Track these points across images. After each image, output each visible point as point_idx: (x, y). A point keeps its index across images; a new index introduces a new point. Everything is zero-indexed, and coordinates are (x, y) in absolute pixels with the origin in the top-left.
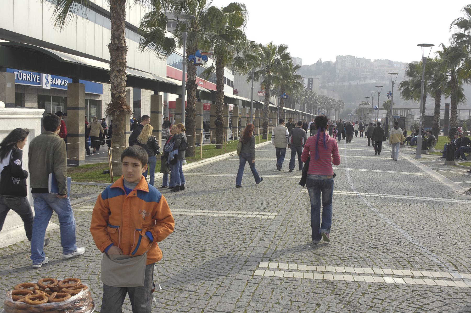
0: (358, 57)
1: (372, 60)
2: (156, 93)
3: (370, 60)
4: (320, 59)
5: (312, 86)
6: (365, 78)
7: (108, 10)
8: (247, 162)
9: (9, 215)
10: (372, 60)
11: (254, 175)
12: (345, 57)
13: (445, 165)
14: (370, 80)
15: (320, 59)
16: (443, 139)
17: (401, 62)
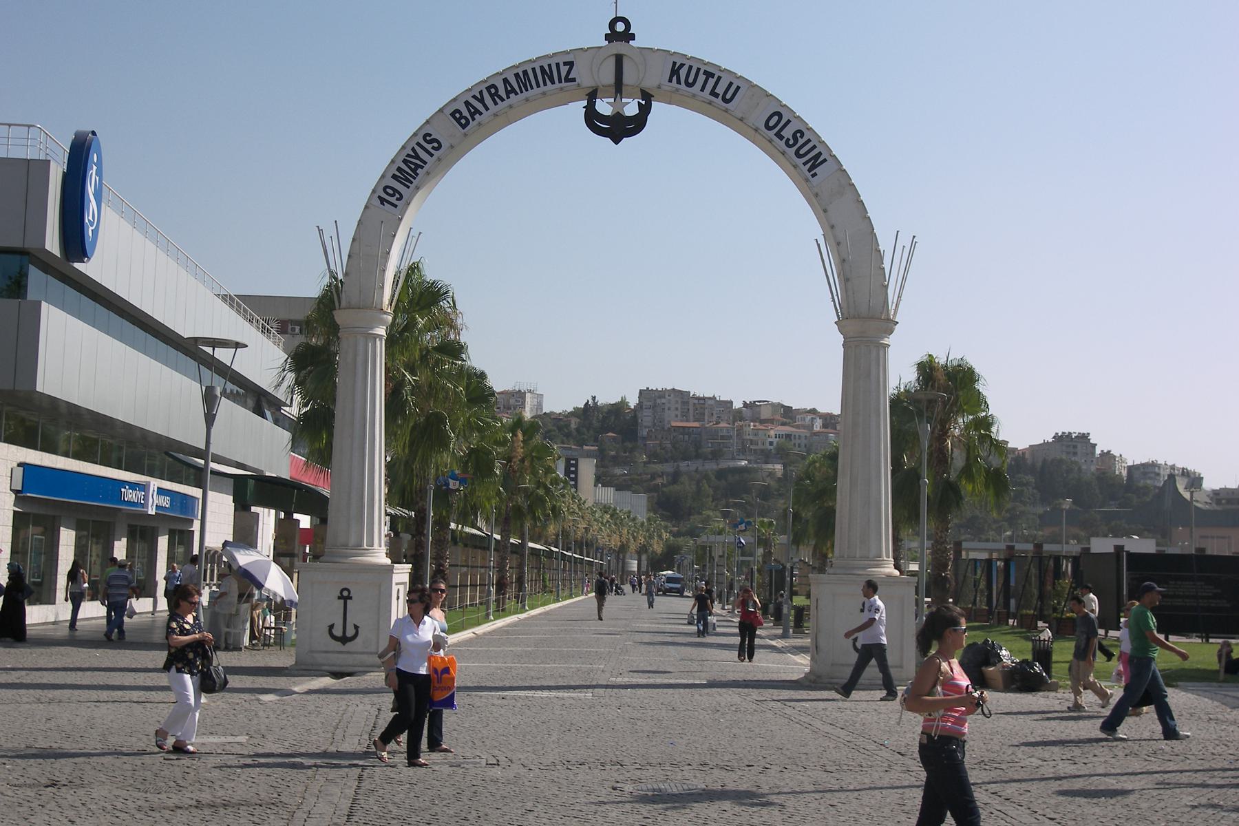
0: (700, 394)
1: (738, 405)
2: (289, 515)
3: (731, 402)
4: (594, 398)
5: (576, 472)
6: (716, 455)
7: (31, 268)
8: (873, 662)
9: (848, 665)
10: (738, 405)
11: (885, 660)
12: (662, 394)
13: (167, 668)
14: (733, 459)
15: (594, 398)
16: (788, 133)
17: (813, 411)
